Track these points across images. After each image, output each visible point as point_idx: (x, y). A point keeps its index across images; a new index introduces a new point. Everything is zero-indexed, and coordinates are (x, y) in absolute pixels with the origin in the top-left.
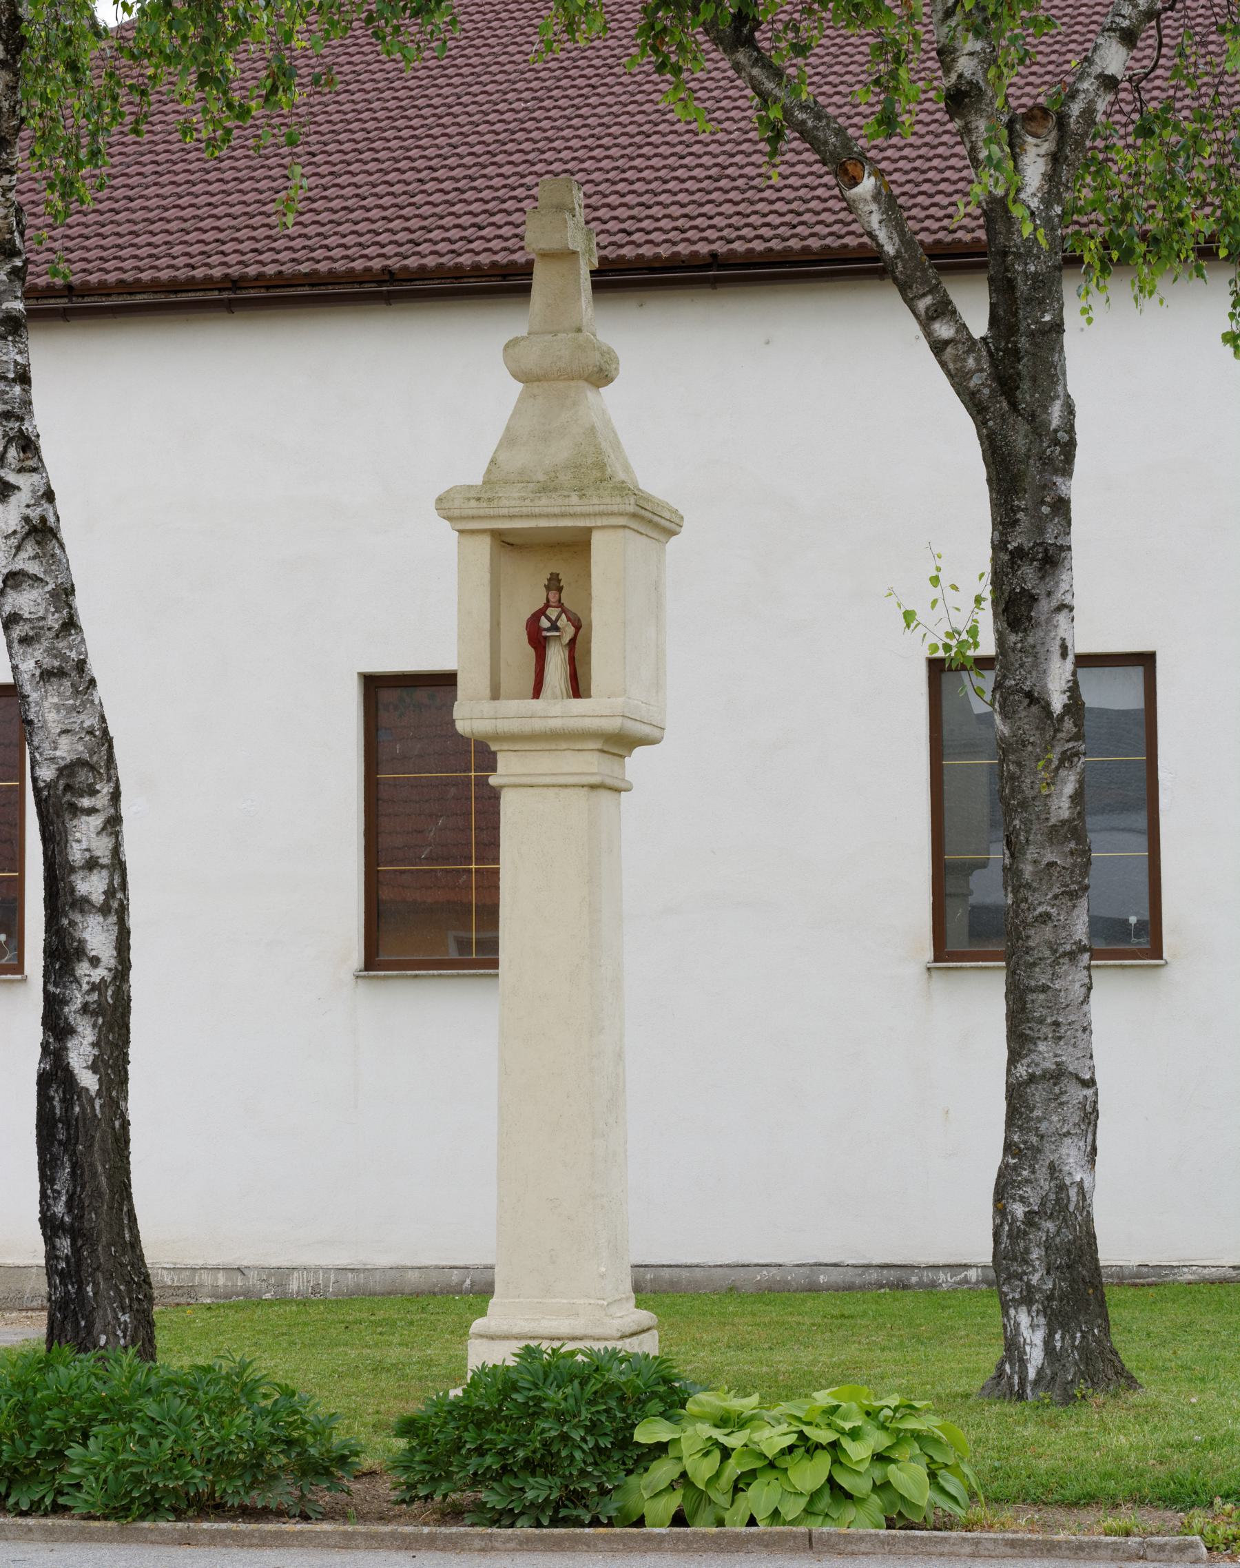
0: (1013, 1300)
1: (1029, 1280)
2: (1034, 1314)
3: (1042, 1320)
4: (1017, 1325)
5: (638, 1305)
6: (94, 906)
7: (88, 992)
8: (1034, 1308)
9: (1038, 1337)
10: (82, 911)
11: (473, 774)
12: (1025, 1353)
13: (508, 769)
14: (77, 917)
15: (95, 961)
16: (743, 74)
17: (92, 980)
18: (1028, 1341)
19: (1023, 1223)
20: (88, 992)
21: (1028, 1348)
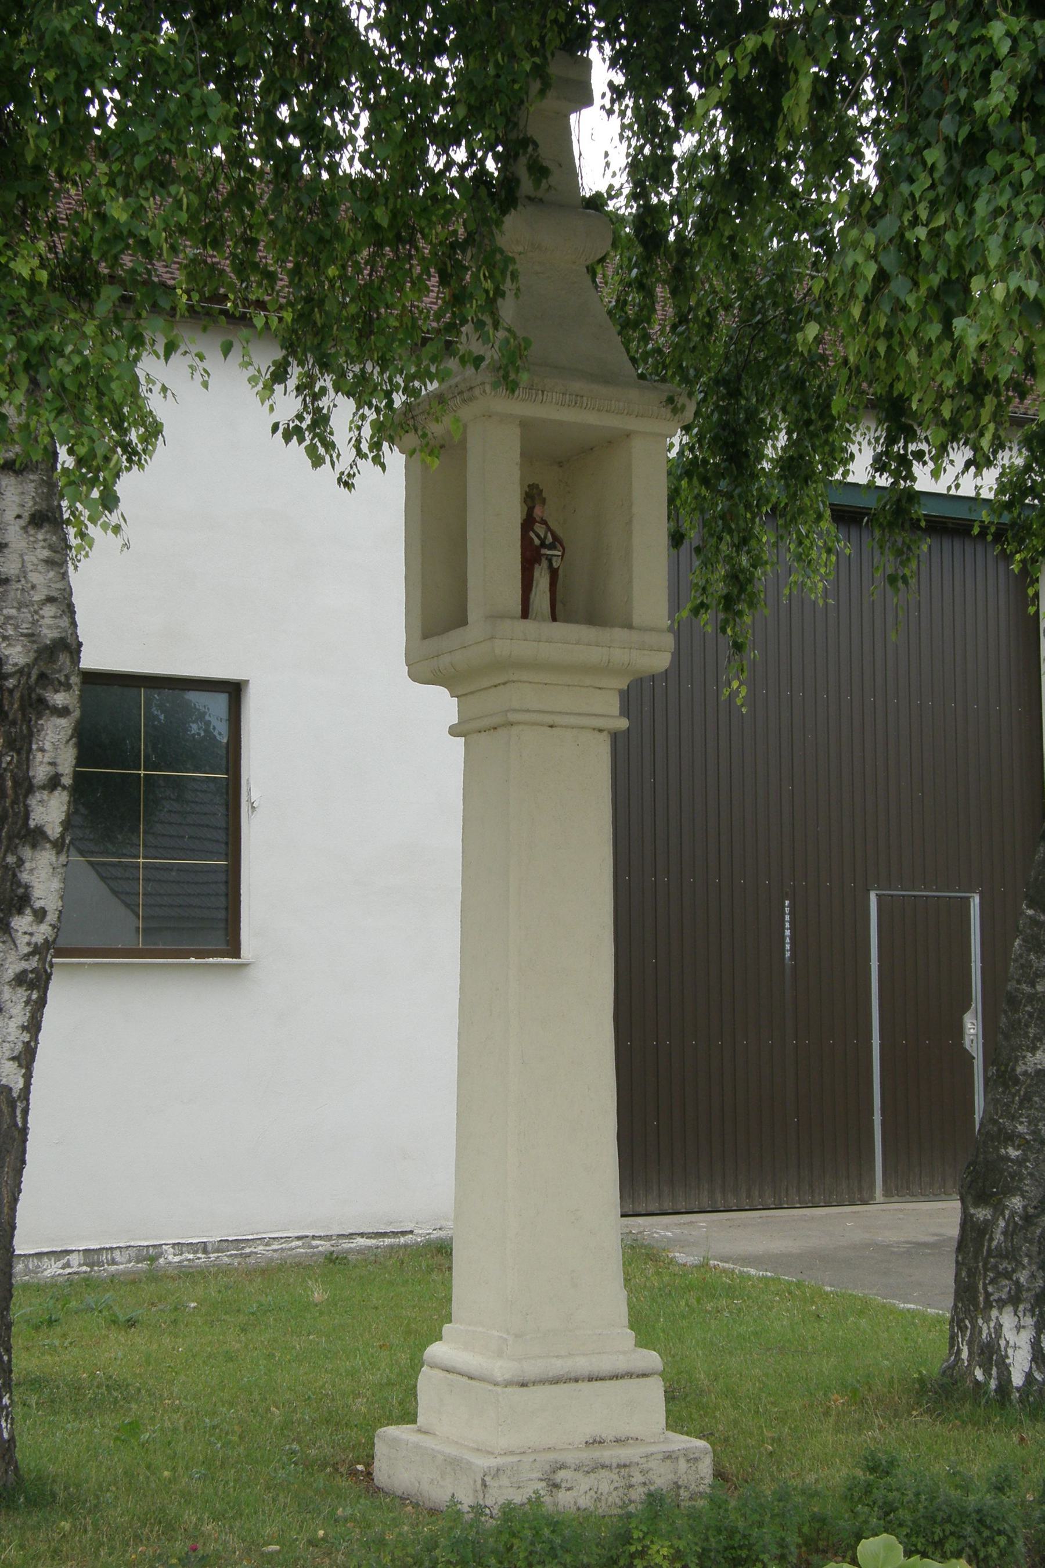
0: (1000, 1300)
1: (1018, 1279)
2: (1021, 1314)
3: (1029, 1321)
4: (999, 1326)
5: (639, 1344)
6: (50, 841)
7: (26, 957)
8: (1021, 1307)
9: (1024, 1340)
10: (34, 846)
11: (142, 772)
12: (1007, 1357)
13: (617, 713)
14: (27, 852)
15: (40, 915)
16: (36, 300)
17: (34, 940)
18: (1011, 1343)
19: (1021, 1218)
20: (26, 957)
21: (1010, 1351)
